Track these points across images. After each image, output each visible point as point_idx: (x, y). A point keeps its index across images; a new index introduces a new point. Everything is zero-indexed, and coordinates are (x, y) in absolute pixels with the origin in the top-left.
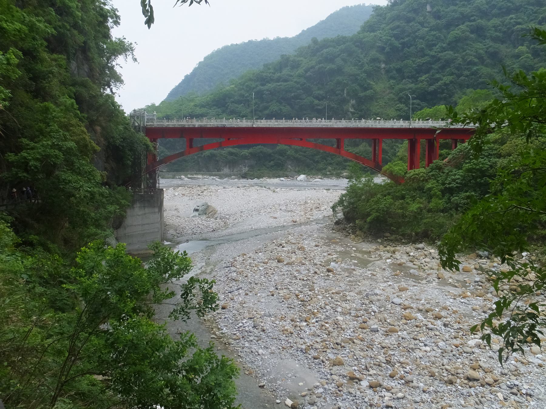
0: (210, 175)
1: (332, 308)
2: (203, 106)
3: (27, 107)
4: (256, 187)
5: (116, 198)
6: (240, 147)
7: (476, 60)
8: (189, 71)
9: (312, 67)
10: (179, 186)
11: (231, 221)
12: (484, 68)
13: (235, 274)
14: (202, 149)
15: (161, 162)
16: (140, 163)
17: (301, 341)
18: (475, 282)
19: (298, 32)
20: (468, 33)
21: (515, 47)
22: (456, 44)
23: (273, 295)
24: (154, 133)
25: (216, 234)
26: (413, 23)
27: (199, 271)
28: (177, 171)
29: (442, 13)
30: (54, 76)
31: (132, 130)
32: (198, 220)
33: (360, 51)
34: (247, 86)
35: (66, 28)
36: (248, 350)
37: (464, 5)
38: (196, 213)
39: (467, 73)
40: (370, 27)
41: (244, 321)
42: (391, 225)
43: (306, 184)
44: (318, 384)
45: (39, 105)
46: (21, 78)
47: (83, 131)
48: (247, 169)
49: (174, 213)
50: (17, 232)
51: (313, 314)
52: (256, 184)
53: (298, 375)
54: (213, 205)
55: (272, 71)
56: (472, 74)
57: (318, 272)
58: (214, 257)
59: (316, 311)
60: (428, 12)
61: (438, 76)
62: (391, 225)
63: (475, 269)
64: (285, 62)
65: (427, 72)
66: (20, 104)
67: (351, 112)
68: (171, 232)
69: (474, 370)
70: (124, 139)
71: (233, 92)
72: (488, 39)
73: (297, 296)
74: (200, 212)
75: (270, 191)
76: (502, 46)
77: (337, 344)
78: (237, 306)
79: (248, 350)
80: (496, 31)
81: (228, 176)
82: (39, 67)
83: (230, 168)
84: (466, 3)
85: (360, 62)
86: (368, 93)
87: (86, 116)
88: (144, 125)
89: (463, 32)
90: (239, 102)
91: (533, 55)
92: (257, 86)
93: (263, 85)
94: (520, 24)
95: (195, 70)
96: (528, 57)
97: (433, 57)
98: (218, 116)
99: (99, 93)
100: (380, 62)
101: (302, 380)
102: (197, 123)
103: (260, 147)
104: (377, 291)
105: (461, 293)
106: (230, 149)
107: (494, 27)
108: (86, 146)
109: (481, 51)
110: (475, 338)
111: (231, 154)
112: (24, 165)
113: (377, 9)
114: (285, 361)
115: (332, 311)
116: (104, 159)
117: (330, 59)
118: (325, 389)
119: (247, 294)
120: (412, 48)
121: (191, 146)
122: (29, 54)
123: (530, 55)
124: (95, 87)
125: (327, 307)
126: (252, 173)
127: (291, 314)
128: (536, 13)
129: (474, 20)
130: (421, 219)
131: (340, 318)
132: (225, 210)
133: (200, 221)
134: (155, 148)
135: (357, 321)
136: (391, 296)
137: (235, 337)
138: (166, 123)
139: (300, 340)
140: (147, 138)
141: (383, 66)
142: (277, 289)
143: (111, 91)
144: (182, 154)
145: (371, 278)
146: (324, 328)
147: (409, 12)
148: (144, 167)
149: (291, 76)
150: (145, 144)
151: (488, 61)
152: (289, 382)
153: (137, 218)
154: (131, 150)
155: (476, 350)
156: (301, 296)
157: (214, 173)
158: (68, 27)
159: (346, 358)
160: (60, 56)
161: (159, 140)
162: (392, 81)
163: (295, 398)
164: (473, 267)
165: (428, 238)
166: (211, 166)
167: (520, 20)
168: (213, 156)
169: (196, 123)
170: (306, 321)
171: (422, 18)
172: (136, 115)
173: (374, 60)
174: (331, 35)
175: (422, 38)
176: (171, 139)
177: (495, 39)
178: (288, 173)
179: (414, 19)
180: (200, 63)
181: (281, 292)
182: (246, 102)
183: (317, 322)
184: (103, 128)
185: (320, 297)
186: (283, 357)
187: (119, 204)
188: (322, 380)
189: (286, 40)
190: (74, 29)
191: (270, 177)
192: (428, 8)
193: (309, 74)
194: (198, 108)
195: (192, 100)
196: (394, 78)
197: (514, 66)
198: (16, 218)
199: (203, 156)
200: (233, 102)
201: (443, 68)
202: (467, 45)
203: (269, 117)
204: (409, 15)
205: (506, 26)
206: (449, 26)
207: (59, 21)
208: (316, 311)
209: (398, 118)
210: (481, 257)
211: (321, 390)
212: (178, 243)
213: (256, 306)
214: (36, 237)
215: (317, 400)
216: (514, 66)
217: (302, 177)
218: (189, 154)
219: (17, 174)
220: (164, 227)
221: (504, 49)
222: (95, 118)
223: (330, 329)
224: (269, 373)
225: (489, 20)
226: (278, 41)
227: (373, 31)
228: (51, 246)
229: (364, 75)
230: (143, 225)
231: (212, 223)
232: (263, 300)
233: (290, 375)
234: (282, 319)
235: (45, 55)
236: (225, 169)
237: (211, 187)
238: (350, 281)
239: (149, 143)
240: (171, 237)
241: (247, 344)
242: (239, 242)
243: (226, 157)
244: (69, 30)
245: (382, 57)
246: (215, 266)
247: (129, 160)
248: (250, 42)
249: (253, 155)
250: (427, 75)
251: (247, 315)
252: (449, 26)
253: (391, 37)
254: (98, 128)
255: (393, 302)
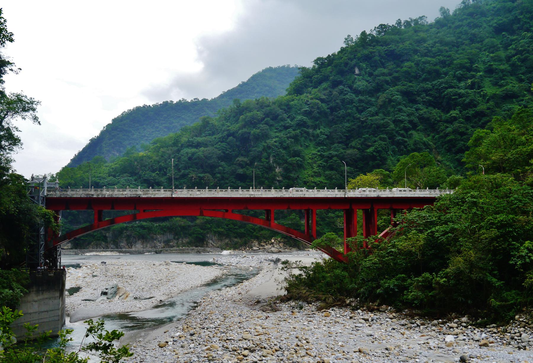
67: (278, 181)
83: (143, 244)
102: (108, 193)
117: (252, 123)
157: (124, 250)
176: (75, 211)
182: (163, 170)
203: (190, 187)
209: (331, 187)
230: (40, 312)
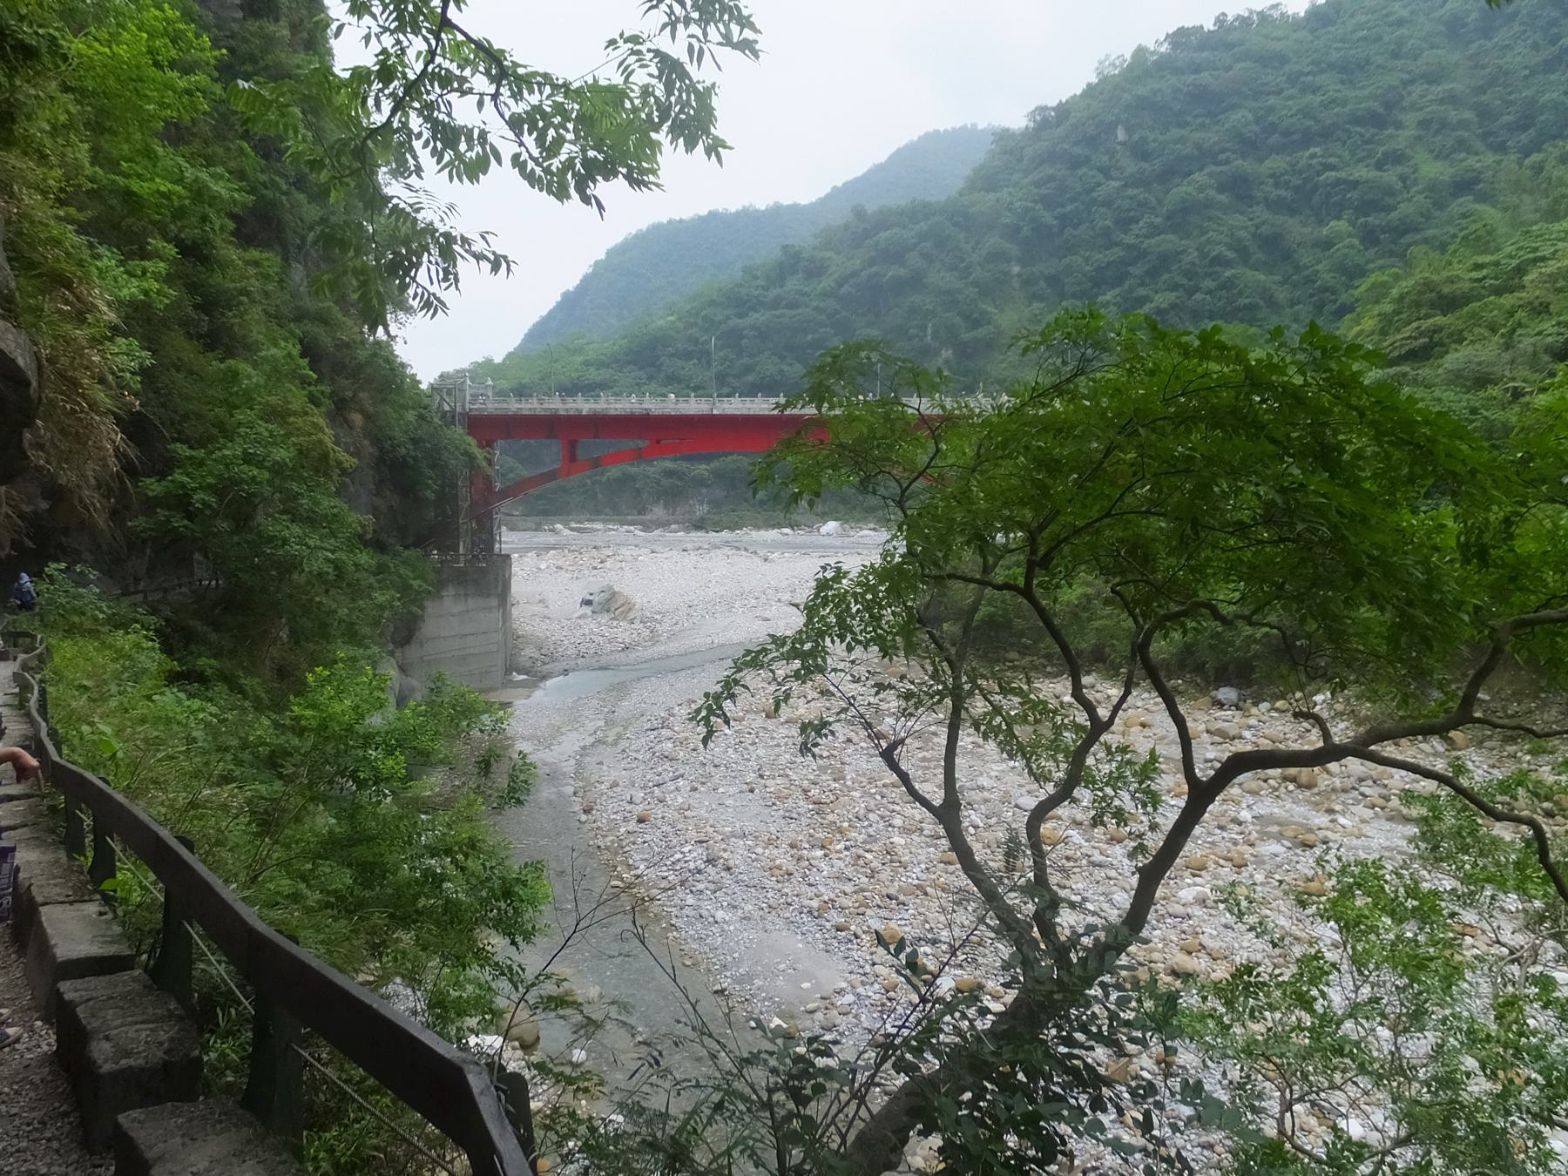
0: (622, 524)
1: (882, 817)
2: (602, 365)
3: (191, 373)
4: (726, 550)
5: (400, 577)
6: (688, 459)
7: (1230, 255)
8: (571, 282)
9: (854, 274)
10: (549, 548)
11: (666, 626)
12: (1250, 273)
13: (670, 745)
14: (596, 463)
15: (505, 494)
16: (456, 497)
17: (810, 891)
18: (1207, 761)
19: (822, 191)
20: (1212, 193)
21: (1321, 222)
22: (1180, 218)
23: (752, 791)
24: (488, 428)
25: (632, 656)
26: (1084, 170)
27: (592, 740)
28: (545, 513)
29: (1154, 145)
30: (253, 301)
31: (436, 420)
32: (590, 626)
33: (962, 236)
34: (705, 318)
35: (279, 189)
36: (692, 913)
37: (1203, 125)
38: (588, 610)
39: (1208, 284)
40: (986, 180)
41: (686, 849)
42: (1022, 634)
43: (838, 544)
44: (844, 985)
45: (214, 365)
46: (175, 305)
47: (315, 425)
48: (706, 508)
49: (538, 608)
50: (167, 649)
51: (841, 831)
52: (727, 544)
53: (800, 966)
54: (626, 591)
55: (761, 282)
56: (1222, 287)
57: (855, 739)
58: (626, 706)
59: (846, 824)
60: (1120, 143)
61: (1142, 292)
62: (1022, 634)
63: (1208, 732)
64: (792, 263)
65: (1118, 281)
66: (174, 365)
68: (529, 651)
69: (1190, 953)
70: (415, 441)
71: (672, 333)
72: (1258, 204)
73: (805, 791)
74: (595, 607)
75: (756, 559)
76: (1291, 221)
77: (890, 897)
78: (671, 815)
79: (692, 913)
80: (1277, 185)
81: (664, 525)
82: (217, 279)
84: (1208, 121)
85: (963, 260)
86: (981, 332)
87: (328, 390)
88: (463, 407)
89: (1201, 189)
90: (688, 356)
91: (1363, 241)
92: (728, 318)
93: (741, 316)
94: (1333, 168)
95: (586, 280)
96: (1352, 247)
97: (1130, 247)
98: (638, 388)
99: (358, 338)
100: (1009, 261)
101: (808, 976)
103: (735, 457)
104: (984, 781)
105: (1172, 785)
106: (669, 464)
107: (1273, 176)
108: (324, 457)
109: (1243, 234)
110: (1195, 885)
111: (669, 474)
112: (181, 501)
113: (1003, 136)
114: (775, 935)
115: (881, 825)
116: (372, 486)
117: (894, 255)
118: (859, 996)
119: (694, 789)
120: (1083, 227)
121: (572, 458)
122: (194, 253)
123: (1356, 242)
124: (350, 323)
125: (871, 816)
126: (716, 518)
127: (791, 832)
128: (1369, 142)
129: (1227, 162)
130: (1090, 619)
131: (896, 839)
132: (654, 602)
133: (598, 628)
134: (490, 462)
135: (936, 846)
136: (1015, 792)
137: (664, 884)
138: (514, 406)
139: (808, 889)
140: (470, 439)
141: (1016, 269)
142: (761, 776)
143: (387, 332)
144: (552, 476)
145: (971, 752)
146: (861, 862)
147: (1076, 143)
148: (465, 505)
149: (806, 294)
150: (466, 454)
151: (1260, 256)
152: (780, 981)
153: (449, 621)
154: (434, 466)
155: (1197, 911)
156: (814, 792)
158: (284, 187)
159: (907, 929)
160: (265, 255)
161: (500, 443)
162: (1036, 305)
163: (792, 1017)
164: (1203, 727)
165: (1104, 662)
166: (625, 503)
167: (1331, 160)
168: (627, 479)
169: (583, 405)
170: (823, 847)
171: (1105, 158)
172: (448, 385)
173: (996, 256)
174: (898, 199)
175: (1107, 204)
177: (1276, 206)
178: (798, 518)
179: (1087, 160)
180: (597, 263)
181: (770, 782)
183: (847, 848)
184: (368, 417)
185: (856, 794)
186: (769, 926)
187: (405, 589)
188: (853, 977)
189: (795, 208)
190: (298, 189)
191: (757, 527)
192: (1121, 135)
193: (846, 289)
194: (592, 370)
195: (579, 351)
196: (1041, 299)
197: (1319, 267)
198: (167, 620)
199: (604, 479)
200: (673, 355)
201: (1153, 274)
202: (1210, 219)
204: (1077, 150)
205: (1300, 172)
206: (1169, 175)
207: (262, 171)
208: (846, 824)
210: (1220, 705)
211: (850, 998)
212: (544, 678)
213: (713, 815)
214: (213, 662)
215: (839, 1020)
216: (1319, 267)
217: (832, 526)
218: (569, 474)
219: (168, 521)
220: (511, 639)
221: (1297, 229)
222: (349, 394)
223: (875, 864)
224: (737, 962)
225: (1261, 160)
226: (776, 211)
227: (994, 190)
228: (246, 682)
229: (972, 291)
231: (623, 632)
232: (730, 802)
233: (782, 966)
234: (769, 843)
235: (232, 253)
236: (656, 509)
237: (623, 550)
238: (924, 759)
239: (476, 450)
240: (528, 664)
241: (690, 900)
242: (683, 673)
243: (658, 482)
244: (286, 194)
245: (1014, 250)
246: (625, 728)
247: (429, 487)
248: (713, 215)
249: (719, 476)
250: (1117, 291)
251: (693, 835)
252: (1169, 175)
253: (1036, 202)
254: (357, 418)
255: (1017, 806)
